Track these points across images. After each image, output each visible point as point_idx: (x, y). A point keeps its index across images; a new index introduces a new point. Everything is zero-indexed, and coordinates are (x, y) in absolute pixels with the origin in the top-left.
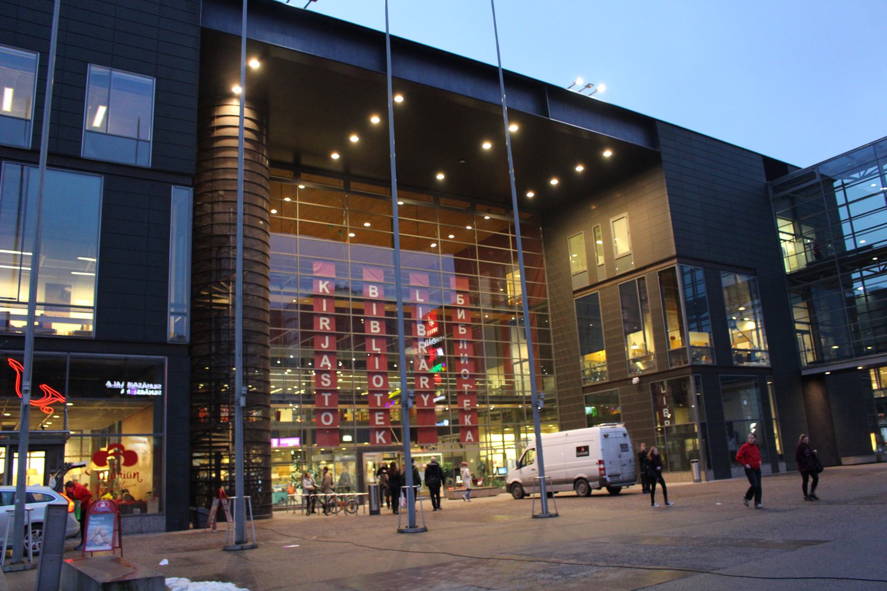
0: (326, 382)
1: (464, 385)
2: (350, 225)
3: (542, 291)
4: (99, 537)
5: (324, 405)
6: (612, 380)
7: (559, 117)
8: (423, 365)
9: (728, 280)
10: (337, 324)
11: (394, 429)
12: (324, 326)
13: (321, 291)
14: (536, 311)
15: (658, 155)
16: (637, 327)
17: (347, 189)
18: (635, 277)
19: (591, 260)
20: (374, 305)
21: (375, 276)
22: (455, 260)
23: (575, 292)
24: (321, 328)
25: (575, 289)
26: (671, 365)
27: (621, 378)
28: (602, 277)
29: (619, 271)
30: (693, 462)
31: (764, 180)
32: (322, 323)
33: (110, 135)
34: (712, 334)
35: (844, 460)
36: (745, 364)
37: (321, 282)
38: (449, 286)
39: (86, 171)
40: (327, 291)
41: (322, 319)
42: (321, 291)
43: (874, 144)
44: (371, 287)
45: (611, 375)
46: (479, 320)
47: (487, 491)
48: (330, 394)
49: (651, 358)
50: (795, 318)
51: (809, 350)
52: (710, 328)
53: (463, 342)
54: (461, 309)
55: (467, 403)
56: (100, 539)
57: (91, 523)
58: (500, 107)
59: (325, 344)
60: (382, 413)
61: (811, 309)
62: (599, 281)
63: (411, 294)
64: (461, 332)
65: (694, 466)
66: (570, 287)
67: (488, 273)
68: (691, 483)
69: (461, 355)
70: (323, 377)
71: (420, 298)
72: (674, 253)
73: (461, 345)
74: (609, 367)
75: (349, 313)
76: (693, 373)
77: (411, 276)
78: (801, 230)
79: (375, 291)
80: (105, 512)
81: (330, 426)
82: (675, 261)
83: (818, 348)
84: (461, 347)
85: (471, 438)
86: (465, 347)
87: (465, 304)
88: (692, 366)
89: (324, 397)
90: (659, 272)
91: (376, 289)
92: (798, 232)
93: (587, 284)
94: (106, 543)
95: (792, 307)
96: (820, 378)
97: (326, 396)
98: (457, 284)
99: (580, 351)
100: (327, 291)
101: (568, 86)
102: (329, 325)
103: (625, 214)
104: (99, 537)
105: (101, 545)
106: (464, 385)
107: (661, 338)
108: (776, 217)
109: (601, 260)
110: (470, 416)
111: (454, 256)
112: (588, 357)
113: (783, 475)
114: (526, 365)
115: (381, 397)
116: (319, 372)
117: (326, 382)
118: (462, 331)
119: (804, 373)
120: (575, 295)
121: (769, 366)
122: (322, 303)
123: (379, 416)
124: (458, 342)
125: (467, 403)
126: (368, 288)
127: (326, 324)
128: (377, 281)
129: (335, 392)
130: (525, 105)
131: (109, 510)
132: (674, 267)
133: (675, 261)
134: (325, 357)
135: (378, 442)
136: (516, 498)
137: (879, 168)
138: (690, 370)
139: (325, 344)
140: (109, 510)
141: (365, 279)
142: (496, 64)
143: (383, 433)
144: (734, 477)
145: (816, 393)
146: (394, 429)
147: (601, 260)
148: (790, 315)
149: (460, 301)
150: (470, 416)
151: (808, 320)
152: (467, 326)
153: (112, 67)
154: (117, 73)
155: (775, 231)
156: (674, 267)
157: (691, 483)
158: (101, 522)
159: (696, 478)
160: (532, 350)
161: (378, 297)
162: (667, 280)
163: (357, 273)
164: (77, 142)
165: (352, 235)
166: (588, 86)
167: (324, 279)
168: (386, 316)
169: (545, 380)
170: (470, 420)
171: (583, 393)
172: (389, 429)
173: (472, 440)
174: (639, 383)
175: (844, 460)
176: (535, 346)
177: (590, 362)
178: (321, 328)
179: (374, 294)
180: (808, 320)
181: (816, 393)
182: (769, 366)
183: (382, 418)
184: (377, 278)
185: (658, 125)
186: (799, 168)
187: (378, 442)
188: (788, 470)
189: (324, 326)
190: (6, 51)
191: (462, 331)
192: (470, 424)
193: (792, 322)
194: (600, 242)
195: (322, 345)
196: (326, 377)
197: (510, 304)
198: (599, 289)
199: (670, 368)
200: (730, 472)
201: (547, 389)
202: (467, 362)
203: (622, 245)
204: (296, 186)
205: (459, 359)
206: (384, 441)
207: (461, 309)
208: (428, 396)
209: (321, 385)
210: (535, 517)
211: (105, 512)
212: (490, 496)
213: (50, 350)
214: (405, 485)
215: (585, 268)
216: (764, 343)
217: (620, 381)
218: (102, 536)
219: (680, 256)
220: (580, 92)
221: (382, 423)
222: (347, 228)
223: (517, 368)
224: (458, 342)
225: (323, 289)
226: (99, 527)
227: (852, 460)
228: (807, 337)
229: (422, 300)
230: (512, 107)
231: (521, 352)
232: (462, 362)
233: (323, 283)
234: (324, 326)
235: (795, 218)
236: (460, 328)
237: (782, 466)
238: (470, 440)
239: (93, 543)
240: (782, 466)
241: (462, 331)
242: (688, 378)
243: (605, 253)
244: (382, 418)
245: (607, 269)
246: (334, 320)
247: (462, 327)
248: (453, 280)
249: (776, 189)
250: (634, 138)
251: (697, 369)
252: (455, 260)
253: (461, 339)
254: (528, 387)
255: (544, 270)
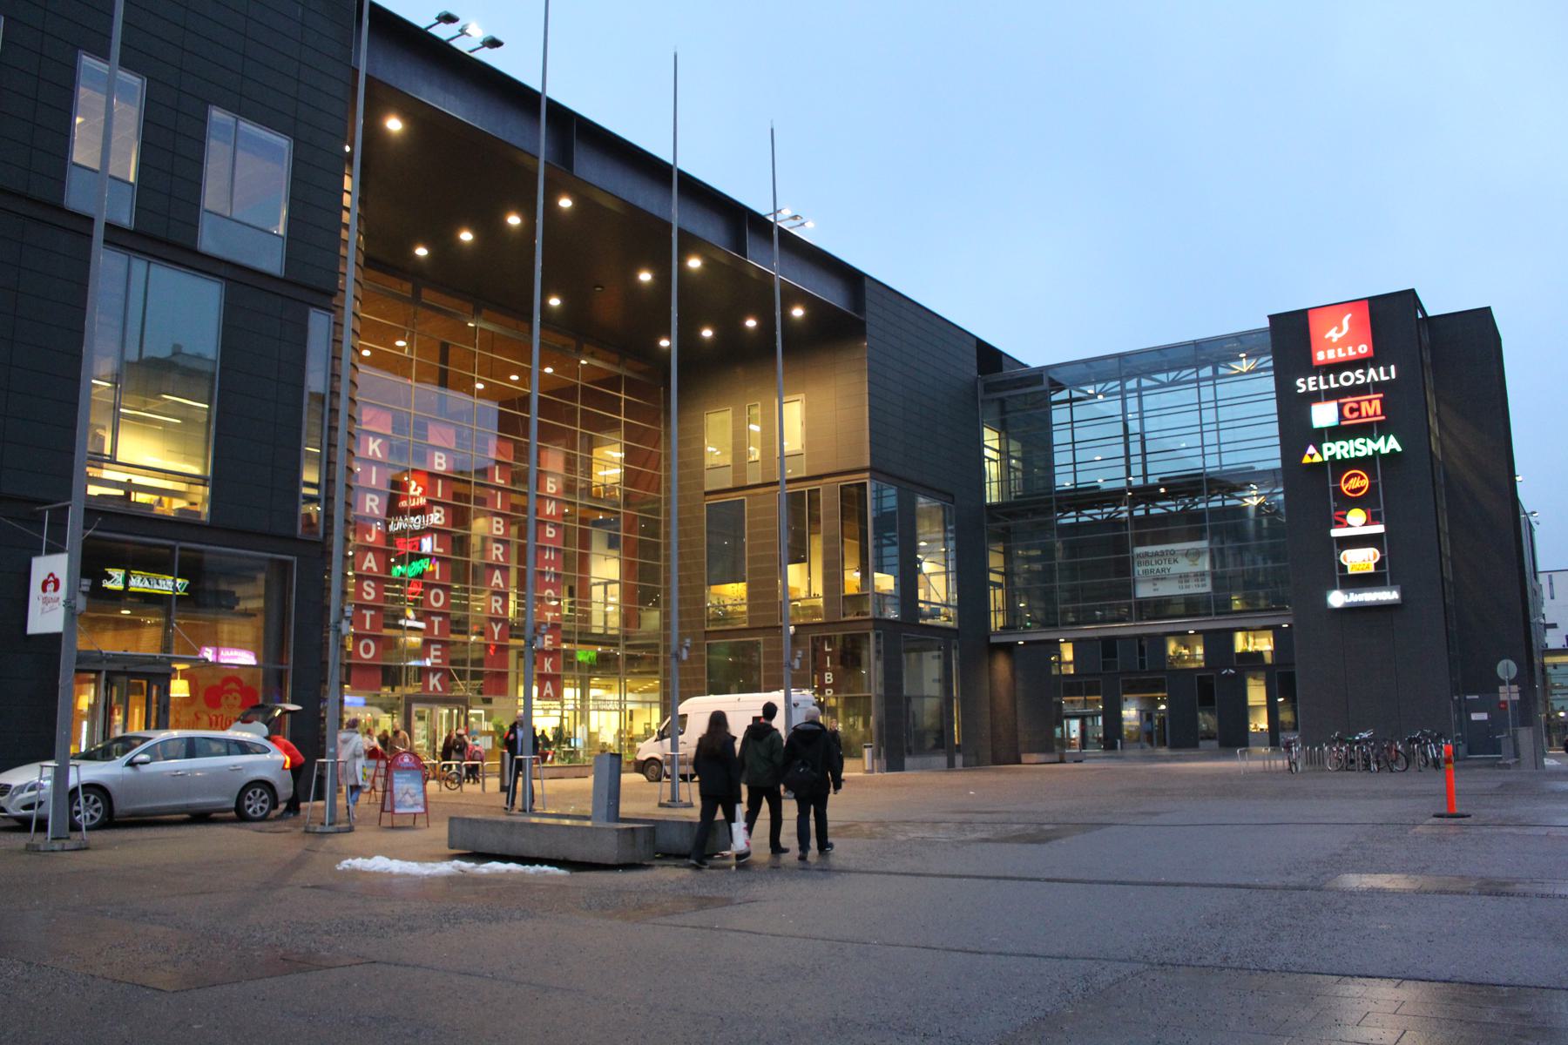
0: (369, 594)
1: (546, 613)
2: (418, 355)
3: (653, 483)
4: (407, 797)
5: (364, 629)
6: (753, 626)
7: (764, 262)
8: (370, 561)
9: (922, 502)
10: (454, 516)
11: (455, 670)
12: (371, 508)
13: (370, 453)
14: (639, 511)
15: (863, 324)
16: (799, 555)
17: (416, 298)
18: (805, 487)
19: (739, 450)
20: (440, 482)
21: (444, 438)
22: (500, 412)
23: (707, 493)
24: (368, 510)
25: (707, 489)
26: (844, 615)
27: (769, 624)
28: (754, 477)
29: (790, 473)
30: (865, 747)
31: (975, 373)
32: (368, 503)
33: (233, 220)
34: (898, 579)
35: (1024, 758)
36: (929, 621)
37: (371, 439)
38: (486, 451)
39: (122, 246)
40: (379, 455)
41: (369, 496)
42: (370, 453)
43: (1120, 356)
44: (437, 454)
45: (751, 618)
46: (467, 499)
47: (578, 769)
48: (373, 612)
49: (369, 531)
50: (991, 566)
51: (999, 611)
52: (896, 569)
53: (550, 548)
54: (552, 499)
55: (549, 639)
56: (409, 800)
57: (396, 780)
58: (669, 226)
59: (370, 536)
60: (439, 646)
61: (1008, 555)
62: (749, 483)
63: (428, 457)
64: (548, 535)
65: (867, 753)
66: (701, 486)
67: (563, 441)
68: (861, 774)
69: (547, 568)
70: (365, 583)
71: (500, 478)
72: (867, 463)
73: (548, 553)
74: (751, 608)
75: (469, 502)
76: (875, 629)
77: (430, 427)
78: (1008, 446)
79: (443, 461)
80: (408, 769)
81: (369, 660)
82: (867, 475)
83: (1011, 610)
84: (547, 557)
85: (550, 691)
86: (553, 558)
87: (556, 493)
88: (875, 620)
89: (365, 615)
90: (841, 487)
91: (444, 459)
92: (1004, 449)
93: (729, 485)
94: (417, 804)
95: (988, 550)
96: (1009, 648)
97: (368, 614)
98: (499, 451)
99: (706, 578)
100: (379, 455)
101: (471, 48)
102: (377, 506)
103: (802, 396)
104: (407, 797)
105: (412, 806)
106: (546, 613)
107: (833, 578)
108: (984, 426)
109: (755, 453)
110: (551, 659)
111: (500, 405)
112: (714, 589)
113: (960, 770)
114: (615, 589)
115: (371, 616)
116: (360, 578)
117: (369, 594)
118: (550, 533)
119: (993, 640)
120: (707, 498)
121: (957, 627)
122: (371, 471)
123: (435, 650)
124: (544, 548)
125: (549, 639)
126: (434, 456)
127: (374, 505)
128: (446, 445)
129: (504, 621)
130: (711, 230)
131: (414, 765)
132: (865, 483)
133: (867, 475)
134: (370, 555)
135: (431, 688)
136: (650, 781)
137: (1120, 384)
138: (871, 625)
139: (370, 536)
140: (414, 765)
141: (430, 442)
142: (539, 89)
143: (439, 675)
144: (908, 770)
145: (1002, 666)
146: (455, 670)
147: (755, 453)
148: (985, 560)
149: (551, 488)
150: (551, 659)
151: (1002, 570)
152: (556, 526)
153: (239, 114)
154: (246, 126)
155: (979, 445)
156: (865, 483)
157: (861, 774)
158: (408, 780)
159: (867, 768)
160: (628, 570)
161: (445, 471)
162: (852, 499)
163: (421, 427)
164: (60, 181)
165: (480, 386)
166: (795, 217)
167: (376, 435)
168: (454, 500)
169: (642, 614)
170: (552, 665)
171: (706, 639)
172: (449, 670)
173: (552, 695)
174: (795, 634)
175: (1024, 758)
176: (632, 564)
177: (719, 596)
178: (368, 510)
179: (440, 465)
180: (1002, 570)
181: (1002, 666)
182: (957, 627)
183: (438, 653)
184: (446, 441)
185: (867, 283)
186: (1026, 366)
187: (431, 688)
188: (964, 765)
189: (371, 508)
190: (100, 67)
191: (550, 533)
192: (550, 671)
193: (986, 570)
194: (755, 428)
195: (367, 536)
196: (369, 586)
197: (594, 494)
198: (747, 495)
199: (842, 619)
200: (903, 761)
201: (643, 627)
202: (553, 580)
203: (794, 439)
204: (579, 361)
205: (543, 574)
206: (440, 689)
207: (552, 499)
208: (500, 625)
209: (361, 597)
210: (661, 805)
211: (408, 769)
212: (576, 777)
213: (237, 547)
214: (323, 757)
215: (728, 461)
216: (953, 593)
217: (764, 628)
218: (411, 796)
219: (874, 470)
220: (470, 52)
221: (439, 661)
222: (412, 360)
223: (597, 593)
224: (544, 548)
225: (374, 451)
226: (406, 786)
227: (1035, 757)
228: (999, 593)
229: (502, 482)
230: (370, 74)
231: (606, 568)
232: (547, 579)
233: (374, 441)
234: (371, 508)
235: (1003, 429)
236: (548, 529)
237: (959, 759)
238: (548, 695)
239: (402, 804)
240: (959, 759)
241: (551, 532)
242: (867, 636)
243: (762, 446)
244: (438, 653)
245: (763, 469)
246: (450, 512)
247: (551, 526)
248: (493, 443)
249: (989, 388)
250: (832, 294)
251: (880, 623)
252: (500, 412)
253: (548, 545)
254: (614, 621)
255: (660, 454)
